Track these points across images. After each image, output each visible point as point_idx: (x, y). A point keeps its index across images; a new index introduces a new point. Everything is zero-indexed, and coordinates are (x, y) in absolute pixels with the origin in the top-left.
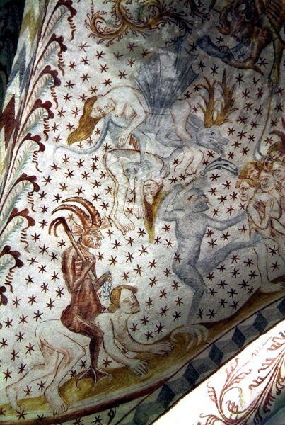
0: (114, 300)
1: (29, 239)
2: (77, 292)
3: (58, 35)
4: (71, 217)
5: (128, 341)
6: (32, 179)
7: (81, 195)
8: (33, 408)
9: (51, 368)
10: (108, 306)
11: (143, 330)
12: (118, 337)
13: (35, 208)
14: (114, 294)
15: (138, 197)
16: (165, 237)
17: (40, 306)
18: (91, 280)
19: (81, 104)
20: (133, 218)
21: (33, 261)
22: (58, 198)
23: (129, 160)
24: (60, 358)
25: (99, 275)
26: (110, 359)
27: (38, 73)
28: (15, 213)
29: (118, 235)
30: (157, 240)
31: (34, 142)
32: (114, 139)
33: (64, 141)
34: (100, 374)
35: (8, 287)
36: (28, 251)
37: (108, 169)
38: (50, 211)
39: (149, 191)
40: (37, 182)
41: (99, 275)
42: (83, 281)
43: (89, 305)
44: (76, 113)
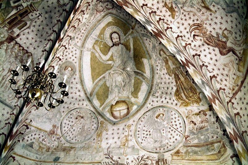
0: (225, 37)
1: (194, 48)
2: (217, 45)
3: (142, 5)
4: (195, 32)
5: (238, 42)
6: (178, 36)
7: (190, 25)
8: (238, 81)
9: (232, 69)
10: (226, 40)
11: (238, 36)
12: (235, 44)
13: (187, 41)
14: (224, 35)
15: (200, 8)
16: (216, 8)
17: (214, 58)
18: (216, 39)
19: (165, 8)
20: (205, 14)
21: (201, 51)
22: (188, 32)
23: (188, 3)
24: (231, 64)
25: (216, 36)
26: (239, 52)
27: (149, 17)
28: (185, 47)
29: (208, 22)
30: (216, 11)
31: (168, 30)
32: (180, 4)
33: (173, 20)
34: (242, 57)
35: (203, 63)
36: (197, 51)
37: (188, 12)
38: (190, 37)
39: (200, 3)
40: (180, 35)
41: (216, 36)
42: (215, 42)
43: (222, 45)
44: (167, 11)
